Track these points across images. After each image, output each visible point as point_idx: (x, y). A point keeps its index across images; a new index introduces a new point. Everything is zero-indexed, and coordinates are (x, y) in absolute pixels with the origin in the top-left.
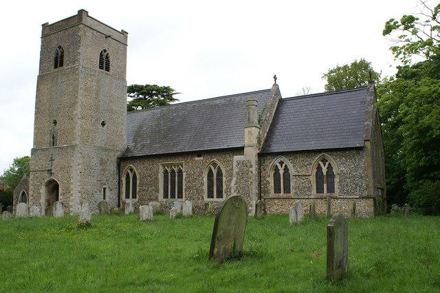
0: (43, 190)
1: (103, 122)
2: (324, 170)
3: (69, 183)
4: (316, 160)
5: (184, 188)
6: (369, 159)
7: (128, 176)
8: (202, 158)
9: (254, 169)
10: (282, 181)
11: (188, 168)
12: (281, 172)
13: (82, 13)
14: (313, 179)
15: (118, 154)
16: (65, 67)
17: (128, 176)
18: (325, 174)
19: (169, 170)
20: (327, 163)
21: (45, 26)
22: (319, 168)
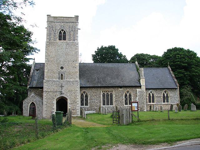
0: (55, 102)
1: (61, 68)
2: (165, 95)
4: (163, 92)
8: (122, 89)
10: (151, 98)
11: (115, 93)
12: (151, 95)
14: (162, 98)
18: (166, 96)
20: (166, 93)
22: (164, 94)
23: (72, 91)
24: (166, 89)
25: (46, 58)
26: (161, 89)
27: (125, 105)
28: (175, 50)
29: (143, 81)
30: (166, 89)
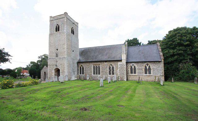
0: (53, 71)
2: (148, 67)
3: (64, 69)
4: (145, 64)
5: (101, 71)
6: (163, 65)
7: (80, 67)
9: (125, 66)
12: (133, 68)
13: (66, 14)
14: (144, 70)
15: (77, 61)
16: (60, 31)
17: (80, 67)
19: (95, 66)
21: (66, 14)
22: (146, 67)
23: (62, 64)
24: (133, 62)
25: (49, 44)
26: (142, 62)
27: (108, 75)
28: (178, 30)
29: (124, 56)
30: (133, 62)
